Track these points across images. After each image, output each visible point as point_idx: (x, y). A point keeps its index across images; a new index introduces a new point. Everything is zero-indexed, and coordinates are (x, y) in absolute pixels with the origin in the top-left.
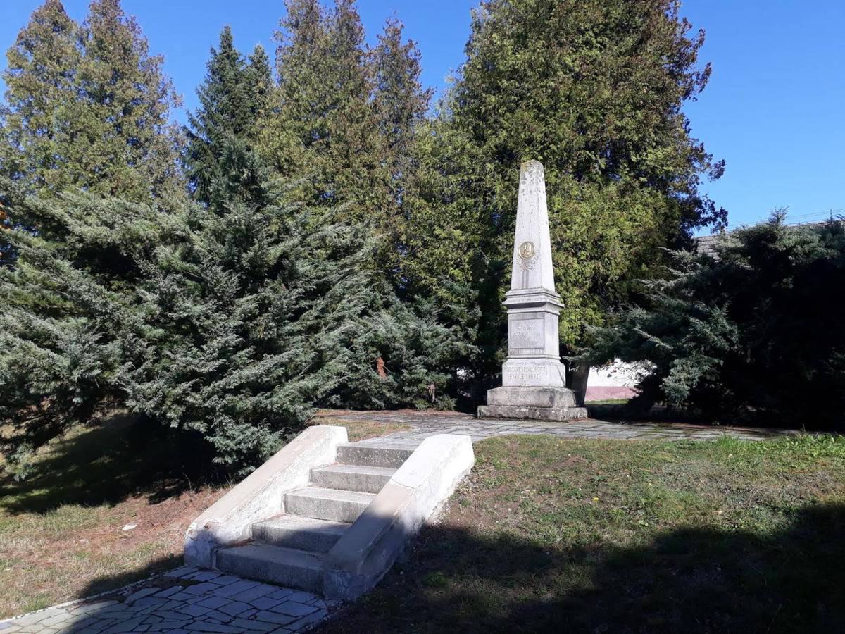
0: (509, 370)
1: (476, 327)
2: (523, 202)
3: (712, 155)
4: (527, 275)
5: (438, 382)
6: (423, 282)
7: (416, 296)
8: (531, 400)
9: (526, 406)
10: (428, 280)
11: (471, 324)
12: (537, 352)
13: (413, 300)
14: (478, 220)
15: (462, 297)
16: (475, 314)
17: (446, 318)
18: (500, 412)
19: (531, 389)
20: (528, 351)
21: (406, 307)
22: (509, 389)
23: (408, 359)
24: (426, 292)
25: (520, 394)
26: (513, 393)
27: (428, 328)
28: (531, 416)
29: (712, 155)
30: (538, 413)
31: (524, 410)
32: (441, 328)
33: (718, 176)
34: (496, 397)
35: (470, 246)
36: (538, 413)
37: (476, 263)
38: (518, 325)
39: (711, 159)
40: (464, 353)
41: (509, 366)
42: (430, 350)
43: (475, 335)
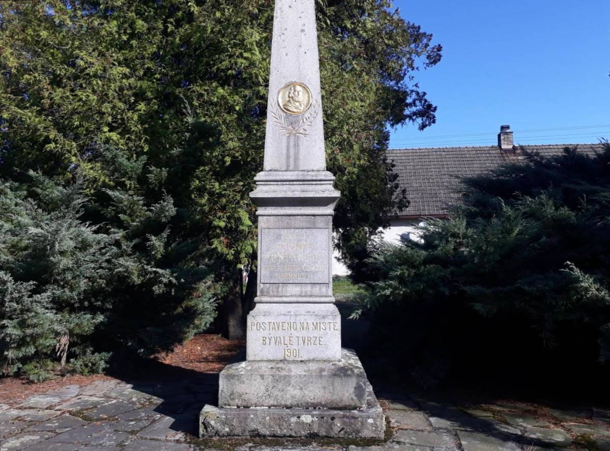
0: (259, 326)
1: (165, 235)
2: (286, 8)
3: (431, 35)
4: (297, 146)
5: (77, 331)
6: (53, 145)
7: (31, 172)
8: (316, 392)
9: (309, 407)
10: (57, 142)
11: (154, 226)
12: (316, 290)
13: (31, 181)
14: (155, 56)
15: (130, 179)
16: (162, 210)
17: (98, 212)
18: (253, 426)
19: (313, 366)
20: (296, 290)
21: (11, 190)
22: (265, 367)
23: (18, 301)
24: (55, 165)
25: (293, 381)
26: (276, 380)
27: (68, 233)
28: (323, 433)
29: (431, 35)
30: (338, 424)
31: (307, 418)
32: (87, 232)
33: (435, 62)
34: (240, 388)
35: (140, 95)
36: (338, 424)
37: (153, 127)
38: (279, 237)
39: (430, 40)
40: (136, 280)
41: (261, 319)
42: (69, 276)
43: (162, 249)
